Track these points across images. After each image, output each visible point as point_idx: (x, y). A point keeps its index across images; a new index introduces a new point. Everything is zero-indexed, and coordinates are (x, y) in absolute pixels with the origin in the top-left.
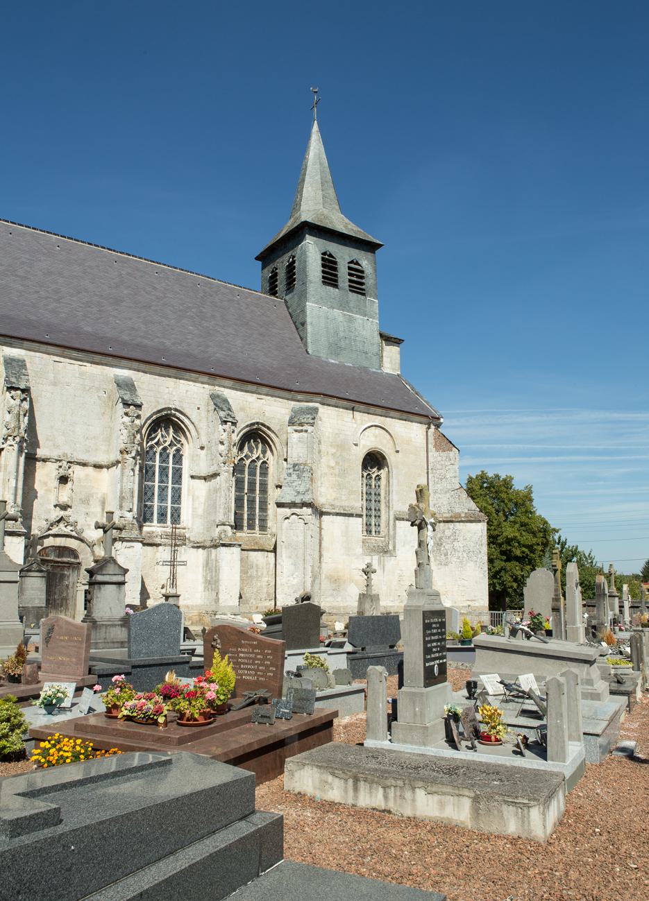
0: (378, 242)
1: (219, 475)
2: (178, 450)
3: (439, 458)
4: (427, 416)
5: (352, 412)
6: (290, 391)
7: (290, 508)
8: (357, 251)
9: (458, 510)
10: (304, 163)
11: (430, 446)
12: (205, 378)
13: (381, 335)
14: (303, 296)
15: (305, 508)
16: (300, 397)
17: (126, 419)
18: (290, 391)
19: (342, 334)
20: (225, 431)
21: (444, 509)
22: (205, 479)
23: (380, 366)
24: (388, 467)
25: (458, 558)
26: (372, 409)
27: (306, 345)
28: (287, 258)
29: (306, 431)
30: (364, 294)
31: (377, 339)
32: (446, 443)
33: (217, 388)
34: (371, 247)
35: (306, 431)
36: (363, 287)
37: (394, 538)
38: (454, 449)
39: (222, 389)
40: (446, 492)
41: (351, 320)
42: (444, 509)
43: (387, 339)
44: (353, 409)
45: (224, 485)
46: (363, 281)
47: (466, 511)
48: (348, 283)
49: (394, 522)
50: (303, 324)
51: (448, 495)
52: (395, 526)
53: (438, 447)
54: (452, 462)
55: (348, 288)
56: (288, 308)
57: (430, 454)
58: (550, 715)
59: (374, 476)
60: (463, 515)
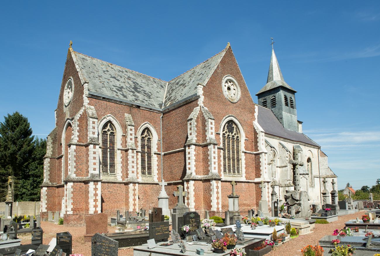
0: (296, 91)
1: (287, 166)
2: (149, 138)
3: (322, 159)
4: (318, 147)
5: (304, 146)
6: (293, 141)
7: (302, 175)
8: (291, 94)
9: (328, 174)
10: (271, 64)
11: (319, 155)
12: (278, 138)
13: (298, 121)
14: (281, 109)
15: (307, 175)
16: (295, 142)
17: (271, 151)
18: (293, 141)
19: (290, 121)
20: (287, 154)
21: (324, 174)
22: (280, 167)
23: (298, 131)
24: (311, 162)
25: (329, 188)
26: (286, 140)
27: (283, 125)
28: (272, 96)
29: (300, 153)
30: (293, 108)
31: (297, 122)
32: (324, 154)
33: (280, 141)
34: (293, 92)
35: (300, 153)
36: (293, 106)
37: (314, 182)
38: (326, 156)
39: (281, 141)
40: (324, 169)
41: (292, 117)
42: (324, 174)
43: (300, 122)
44: (305, 146)
45: (289, 169)
46: (293, 104)
47: (330, 174)
48: (290, 105)
49: (314, 178)
50: (281, 118)
51: (325, 170)
52: (314, 179)
53: (321, 156)
54: (326, 160)
55: (290, 107)
56: (273, 113)
57: (319, 158)
58: (60, 226)
59: (109, 133)
60: (330, 176)
